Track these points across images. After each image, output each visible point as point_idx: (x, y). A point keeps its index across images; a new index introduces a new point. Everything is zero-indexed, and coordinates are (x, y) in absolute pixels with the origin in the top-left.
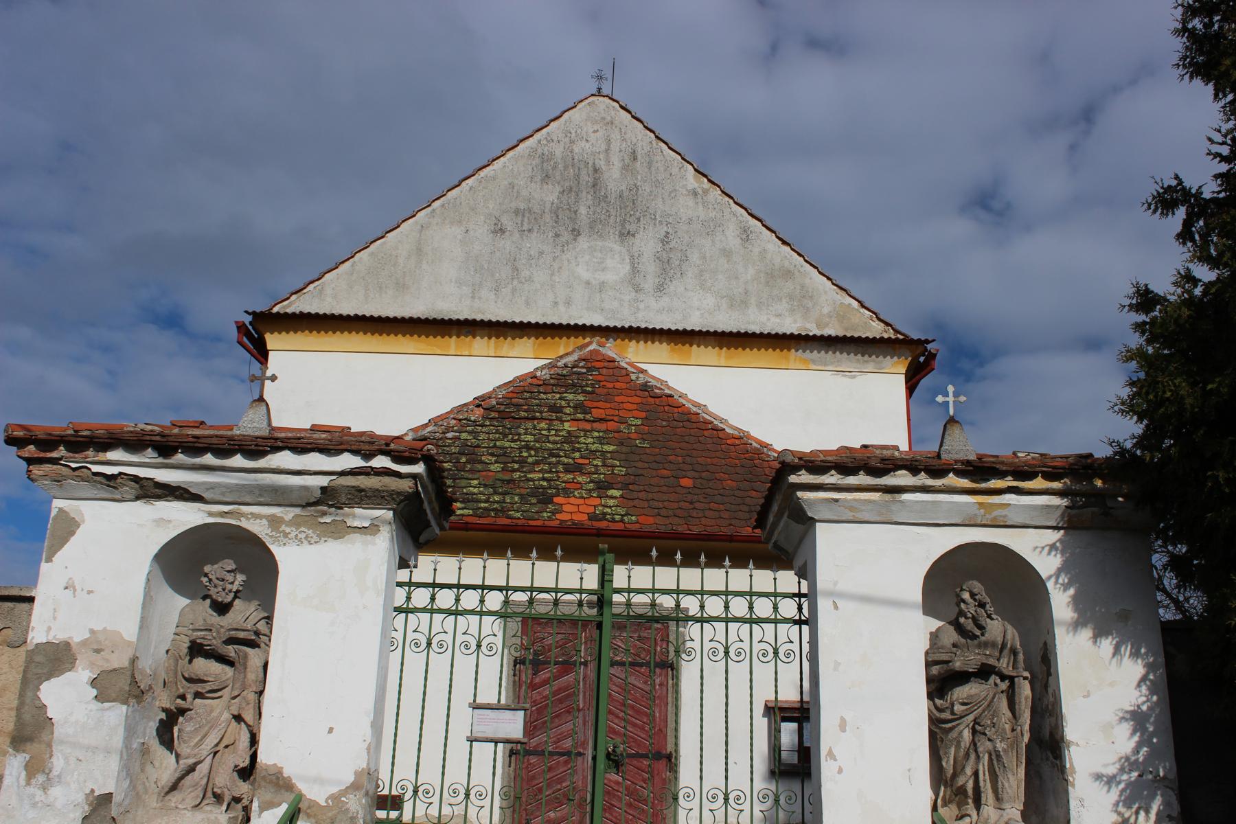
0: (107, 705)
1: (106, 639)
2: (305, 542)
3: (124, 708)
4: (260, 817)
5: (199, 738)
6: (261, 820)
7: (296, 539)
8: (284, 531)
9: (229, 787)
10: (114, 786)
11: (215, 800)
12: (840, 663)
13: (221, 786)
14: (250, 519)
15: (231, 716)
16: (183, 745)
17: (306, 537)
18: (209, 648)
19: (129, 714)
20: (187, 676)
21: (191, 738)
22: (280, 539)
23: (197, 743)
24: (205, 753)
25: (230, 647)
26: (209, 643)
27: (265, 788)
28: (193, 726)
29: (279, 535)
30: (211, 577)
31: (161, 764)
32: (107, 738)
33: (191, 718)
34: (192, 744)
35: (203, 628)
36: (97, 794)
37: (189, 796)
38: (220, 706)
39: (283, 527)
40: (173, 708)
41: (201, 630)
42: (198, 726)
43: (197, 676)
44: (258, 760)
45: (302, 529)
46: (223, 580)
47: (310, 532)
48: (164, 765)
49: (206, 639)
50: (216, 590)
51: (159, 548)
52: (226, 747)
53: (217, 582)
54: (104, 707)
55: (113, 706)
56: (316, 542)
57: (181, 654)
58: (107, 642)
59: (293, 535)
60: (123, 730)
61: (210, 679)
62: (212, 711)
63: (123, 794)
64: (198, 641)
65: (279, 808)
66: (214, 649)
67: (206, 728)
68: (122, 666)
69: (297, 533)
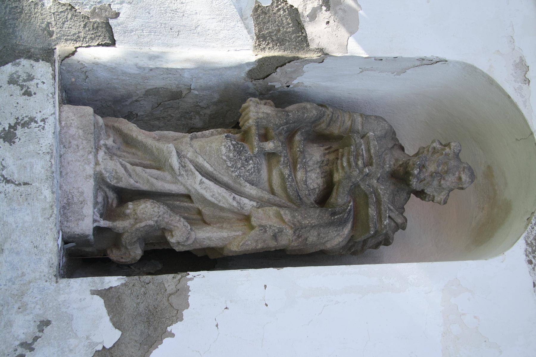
6: (89, 296)
28: (228, 157)
44: (192, 274)
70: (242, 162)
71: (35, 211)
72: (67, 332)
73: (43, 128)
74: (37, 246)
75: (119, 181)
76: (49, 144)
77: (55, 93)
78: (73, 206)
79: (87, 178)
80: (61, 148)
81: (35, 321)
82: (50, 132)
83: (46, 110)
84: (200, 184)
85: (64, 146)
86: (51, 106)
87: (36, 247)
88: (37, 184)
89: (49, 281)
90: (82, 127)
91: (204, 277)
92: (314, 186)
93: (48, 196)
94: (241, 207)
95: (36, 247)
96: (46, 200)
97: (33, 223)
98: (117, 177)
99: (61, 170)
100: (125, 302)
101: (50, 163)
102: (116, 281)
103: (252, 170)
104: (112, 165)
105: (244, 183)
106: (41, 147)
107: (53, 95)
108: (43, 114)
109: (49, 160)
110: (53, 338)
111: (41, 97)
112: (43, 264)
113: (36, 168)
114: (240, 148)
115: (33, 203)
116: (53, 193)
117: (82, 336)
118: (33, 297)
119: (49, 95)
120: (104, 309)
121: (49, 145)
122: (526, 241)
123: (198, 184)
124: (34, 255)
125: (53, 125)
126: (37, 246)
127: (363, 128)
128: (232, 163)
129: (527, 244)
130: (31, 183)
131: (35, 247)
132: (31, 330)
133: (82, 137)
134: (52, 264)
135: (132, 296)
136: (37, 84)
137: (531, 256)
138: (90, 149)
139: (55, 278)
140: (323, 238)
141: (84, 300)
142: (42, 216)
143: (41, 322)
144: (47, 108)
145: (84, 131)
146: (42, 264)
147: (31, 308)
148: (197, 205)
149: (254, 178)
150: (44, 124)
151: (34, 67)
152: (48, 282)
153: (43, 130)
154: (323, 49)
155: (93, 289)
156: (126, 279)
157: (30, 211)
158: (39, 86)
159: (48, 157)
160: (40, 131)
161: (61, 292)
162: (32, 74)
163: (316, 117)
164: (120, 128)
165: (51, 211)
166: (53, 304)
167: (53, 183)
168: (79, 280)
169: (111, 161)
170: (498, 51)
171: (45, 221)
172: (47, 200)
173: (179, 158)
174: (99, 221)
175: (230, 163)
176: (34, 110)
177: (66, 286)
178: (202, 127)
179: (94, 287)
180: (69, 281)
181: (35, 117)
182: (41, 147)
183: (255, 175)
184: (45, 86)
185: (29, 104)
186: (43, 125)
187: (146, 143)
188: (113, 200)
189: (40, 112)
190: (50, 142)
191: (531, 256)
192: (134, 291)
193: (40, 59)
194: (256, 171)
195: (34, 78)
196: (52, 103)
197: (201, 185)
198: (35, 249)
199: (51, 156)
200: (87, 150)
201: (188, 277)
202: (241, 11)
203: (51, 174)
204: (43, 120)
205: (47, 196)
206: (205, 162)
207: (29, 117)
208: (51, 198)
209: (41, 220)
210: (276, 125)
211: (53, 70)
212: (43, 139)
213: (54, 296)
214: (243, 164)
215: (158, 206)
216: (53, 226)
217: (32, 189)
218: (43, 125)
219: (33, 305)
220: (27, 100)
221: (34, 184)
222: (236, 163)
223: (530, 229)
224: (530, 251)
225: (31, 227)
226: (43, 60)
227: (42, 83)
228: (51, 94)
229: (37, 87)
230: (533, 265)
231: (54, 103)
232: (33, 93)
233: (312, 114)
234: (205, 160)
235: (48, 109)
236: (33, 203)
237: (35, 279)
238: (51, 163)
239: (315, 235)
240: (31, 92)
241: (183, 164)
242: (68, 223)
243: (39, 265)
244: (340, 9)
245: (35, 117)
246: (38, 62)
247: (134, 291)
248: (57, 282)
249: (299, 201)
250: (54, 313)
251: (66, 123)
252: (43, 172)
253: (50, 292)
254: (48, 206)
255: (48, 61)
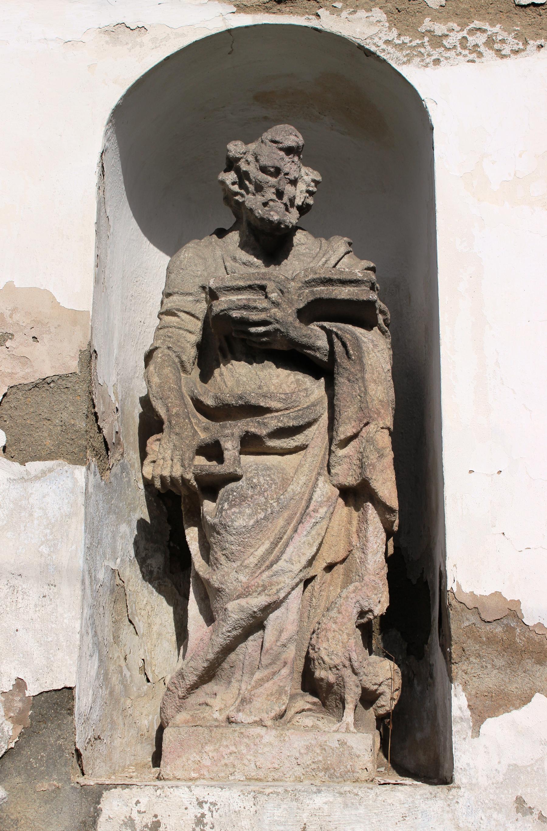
0: (35, 467)
1: (15, 310)
2: (488, 54)
3: (80, 472)
4: (476, 732)
5: (267, 545)
6: (482, 740)
7: (464, 48)
8: (429, 31)
9: (356, 664)
10: (74, 669)
11: (316, 700)
12: (140, 803)
13: (337, 661)
14: (341, 10)
15: (337, 492)
16: (226, 566)
17: (490, 42)
18: (262, 329)
19: (91, 490)
20: (210, 402)
21: (246, 546)
22: (422, 50)
23: (263, 559)
24: (287, 581)
25: (314, 327)
26: (262, 316)
27: (479, 656)
28: (250, 516)
29: (418, 41)
30: (244, 167)
31: (150, 625)
32: (44, 549)
33: (243, 498)
34: (252, 561)
35: (241, 283)
36: (32, 690)
37: (261, 690)
38: (305, 469)
39: (427, 24)
40: (189, 476)
41: (239, 289)
42: (262, 515)
43: (241, 398)
44: (450, 585)
45: (477, 24)
46: (277, 172)
47: (497, 28)
48: (155, 628)
49: (255, 308)
50: (260, 198)
51: (123, 91)
52: (329, 568)
53: (262, 177)
54: (28, 473)
55: (51, 470)
56: (516, 52)
57: (184, 358)
58: (17, 317)
59: (454, 39)
60: (82, 527)
61: (274, 404)
62: (286, 482)
63: (91, 692)
64: (235, 314)
65: (525, 708)
66: (277, 330)
67: (281, 522)
68: (63, 372)
69: (465, 33)
70: (257, 495)
71: (348, 819)
72: (534, 773)
73: (214, 804)
74: (403, 817)
75: (284, 691)
76: (239, 796)
77: (155, 786)
78: (329, 762)
79: (284, 740)
80: (235, 779)
81: (517, 820)
82: (220, 793)
83: (183, 800)
84: (293, 564)
85: (231, 774)
86: (177, 792)
87: (404, 817)
88: (305, 815)
89: (457, 798)
90: (200, 746)
91: (455, 565)
92: (292, 382)
93: (325, 800)
94: (328, 501)
95: (404, 817)
96: (331, 803)
97: (367, 823)
98: (278, 694)
99: (270, 779)
100: (491, 686)
101: (271, 795)
102: (459, 699)
103: (268, 479)
104: (259, 700)
105: (288, 493)
106: (244, 808)
107: (158, 789)
108: (191, 804)
109: (265, 796)
110: (541, 795)
111: (161, 806)
112: (430, 807)
113: (279, 816)
114: (234, 496)
115: (335, 821)
116: (319, 791)
117: (541, 752)
118: (480, 823)
119: (158, 794)
120: (501, 717)
121: (242, 796)
122: (404, 63)
123: (292, 567)
124: (415, 821)
125: (209, 790)
126: (403, 817)
127: (191, 294)
128: (259, 511)
129: (409, 61)
130: (303, 824)
131: (405, 819)
132: (529, 825)
133: (217, 746)
134: (431, 793)
135: (482, 676)
136: (139, 812)
137: (428, 60)
138: (236, 734)
139: (452, 791)
140: (379, 374)
141: (486, 748)
142: (357, 809)
143: (518, 812)
144: (181, 798)
145: (206, 743)
146: (431, 809)
147: (496, 825)
148: (319, 570)
149: (279, 478)
150: (206, 803)
151: (111, 816)
152: (458, 801)
153: (217, 805)
154: (80, 350)
155: (470, 733)
156: (456, 684)
157: (348, 827)
158: (143, 810)
159: (262, 798)
160: (218, 809)
161: (474, 781)
162: (123, 820)
163: (174, 369)
164: (189, 686)
165: (348, 795)
166: (491, 793)
167: (303, 792)
168: (456, 754)
169: (254, 702)
170: (89, 67)
171: (364, 803)
172: (331, 801)
173: (251, 595)
174: (347, 724)
175: (260, 513)
176: (184, 818)
177: (464, 774)
178: (164, 555)
179: (467, 733)
180: (458, 769)
181: (196, 816)
182: (244, 808)
183: (274, 474)
184: (144, 800)
185: (173, 825)
186: (208, 805)
187: (221, 645)
188: (306, 702)
189: (186, 809)
190: (236, 795)
191: (428, 60)
192: (475, 673)
193: (97, 807)
194: (268, 472)
195: (130, 817)
196: (172, 790)
197: (294, 562)
198: (407, 819)
199: (260, 793)
200: (237, 739)
201: (455, 590)
202: (14, 479)
203: (290, 794)
204: (200, 804)
205: (324, 801)
206: (256, 553)
207: (194, 826)
208: (328, 795)
209: (362, 810)
210: (194, 436)
211: (116, 788)
212: (231, 805)
213: (479, 792)
214: (260, 494)
215: (324, 632)
216: (372, 792)
217: (313, 823)
218: (208, 805)
219: (493, 823)
220: (166, 828)
221: (305, 820)
222: (258, 504)
223: (384, 55)
224: (419, 59)
225: (373, 826)
226: (99, 803)
227: (138, 805)
228: (156, 791)
229: (145, 812)
230: (442, 59)
231: (172, 787)
232: (155, 819)
233: (170, 375)
234: (252, 554)
235: (182, 796)
236: (335, 821)
237: (454, 819)
238: (272, 793)
239: (374, 387)
240: (153, 822)
241: (260, 589)
242: (357, 770)
243: (432, 813)
244: (10, 317)
245: (196, 816)
246: (102, 811)
247: (475, 673)
248: (459, 787)
249: (318, 408)
250: (506, 791)
251: (194, 770)
252: (285, 806)
253: (473, 798)
254: (340, 799)
255: (100, 795)
